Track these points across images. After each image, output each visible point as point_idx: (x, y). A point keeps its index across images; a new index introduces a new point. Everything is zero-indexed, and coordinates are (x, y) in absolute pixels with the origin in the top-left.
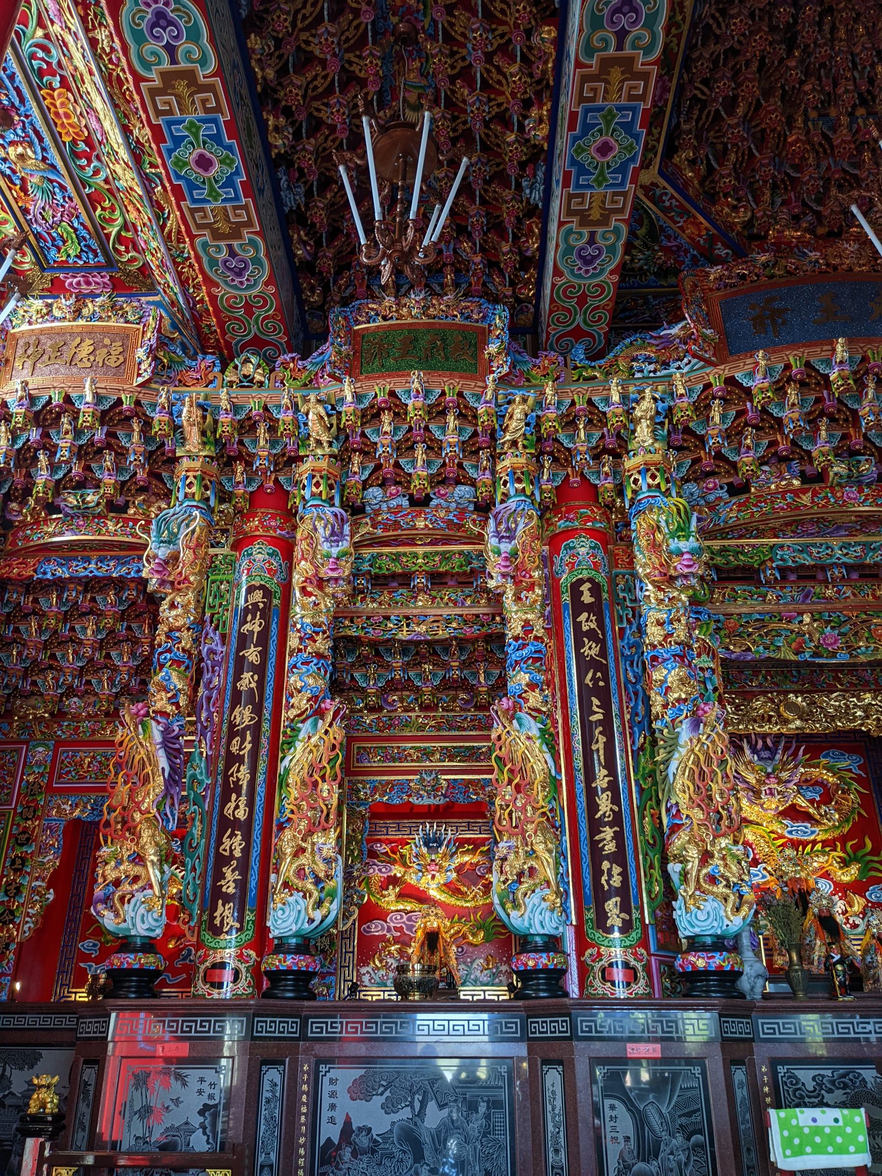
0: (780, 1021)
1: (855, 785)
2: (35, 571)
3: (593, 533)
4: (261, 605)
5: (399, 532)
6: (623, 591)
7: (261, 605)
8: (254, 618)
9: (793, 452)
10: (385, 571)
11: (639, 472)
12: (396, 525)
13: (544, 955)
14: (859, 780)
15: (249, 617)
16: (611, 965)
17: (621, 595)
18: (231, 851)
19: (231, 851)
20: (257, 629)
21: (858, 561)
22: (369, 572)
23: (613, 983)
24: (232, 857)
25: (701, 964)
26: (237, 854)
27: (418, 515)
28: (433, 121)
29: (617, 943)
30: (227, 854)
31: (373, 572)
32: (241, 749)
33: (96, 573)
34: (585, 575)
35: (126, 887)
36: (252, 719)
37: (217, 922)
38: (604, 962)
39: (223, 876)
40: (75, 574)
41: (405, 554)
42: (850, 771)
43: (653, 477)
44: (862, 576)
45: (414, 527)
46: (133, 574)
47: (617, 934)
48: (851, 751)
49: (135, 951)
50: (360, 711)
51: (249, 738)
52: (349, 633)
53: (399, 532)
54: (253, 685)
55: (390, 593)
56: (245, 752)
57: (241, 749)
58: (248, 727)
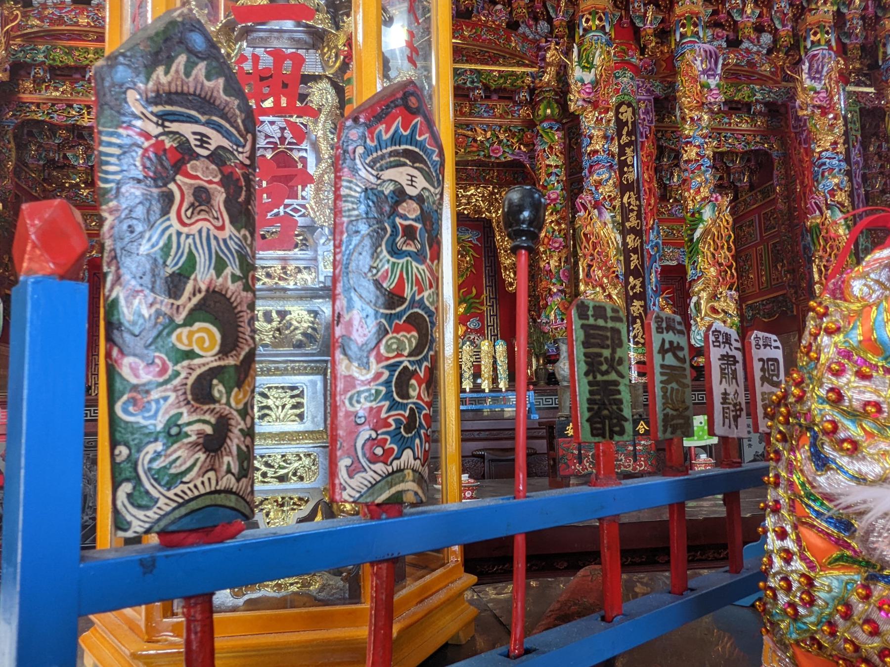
1: (472, 252)
5: (63, 27)
6: (643, 113)
9: (727, 21)
10: (58, 63)
11: (590, 14)
12: (60, 20)
14: (475, 248)
17: (642, 117)
22: (44, 62)
27: (81, 12)
28: (868, 93)
31: (47, 62)
41: (77, 49)
42: (470, 242)
43: (600, 19)
44: (500, 98)
45: (76, 24)
46: (468, 85)
48: (473, 228)
50: (77, 184)
52: (35, 117)
53: (63, 27)
55: (72, 83)
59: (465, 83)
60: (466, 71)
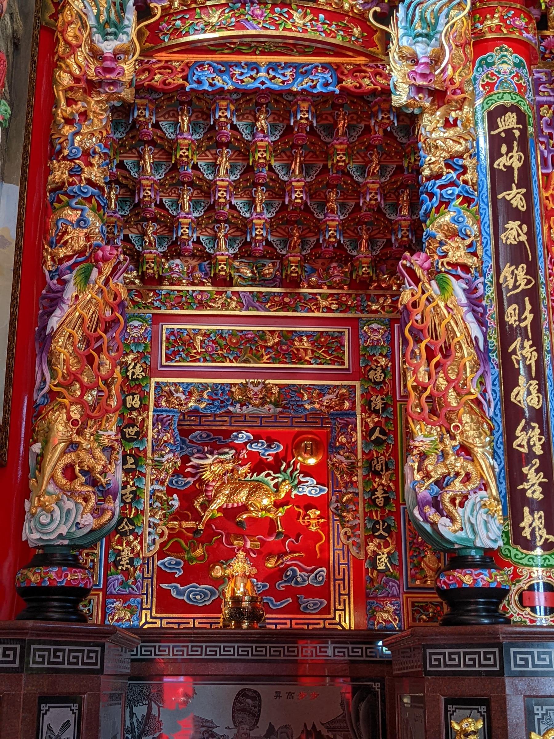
0: (318, 646)
2: (185, 78)
3: (520, 46)
4: (517, 133)
7: (517, 133)
8: (510, 150)
13: (486, 572)
15: (504, 149)
16: (531, 588)
18: (530, 447)
19: (530, 447)
20: (517, 165)
21: (285, 87)
23: (533, 609)
24: (531, 455)
25: (468, 580)
26: (538, 450)
29: (539, 561)
30: (525, 450)
32: (520, 320)
33: (269, 85)
34: (508, 100)
35: (458, 486)
36: (529, 282)
37: (527, 533)
38: (524, 585)
39: (524, 478)
40: (241, 86)
46: (319, 89)
47: (539, 551)
49: (474, 565)
51: (528, 307)
54: (523, 238)
56: (528, 322)
57: (520, 320)
58: (524, 293)
59: (315, 87)
60: (316, 67)
